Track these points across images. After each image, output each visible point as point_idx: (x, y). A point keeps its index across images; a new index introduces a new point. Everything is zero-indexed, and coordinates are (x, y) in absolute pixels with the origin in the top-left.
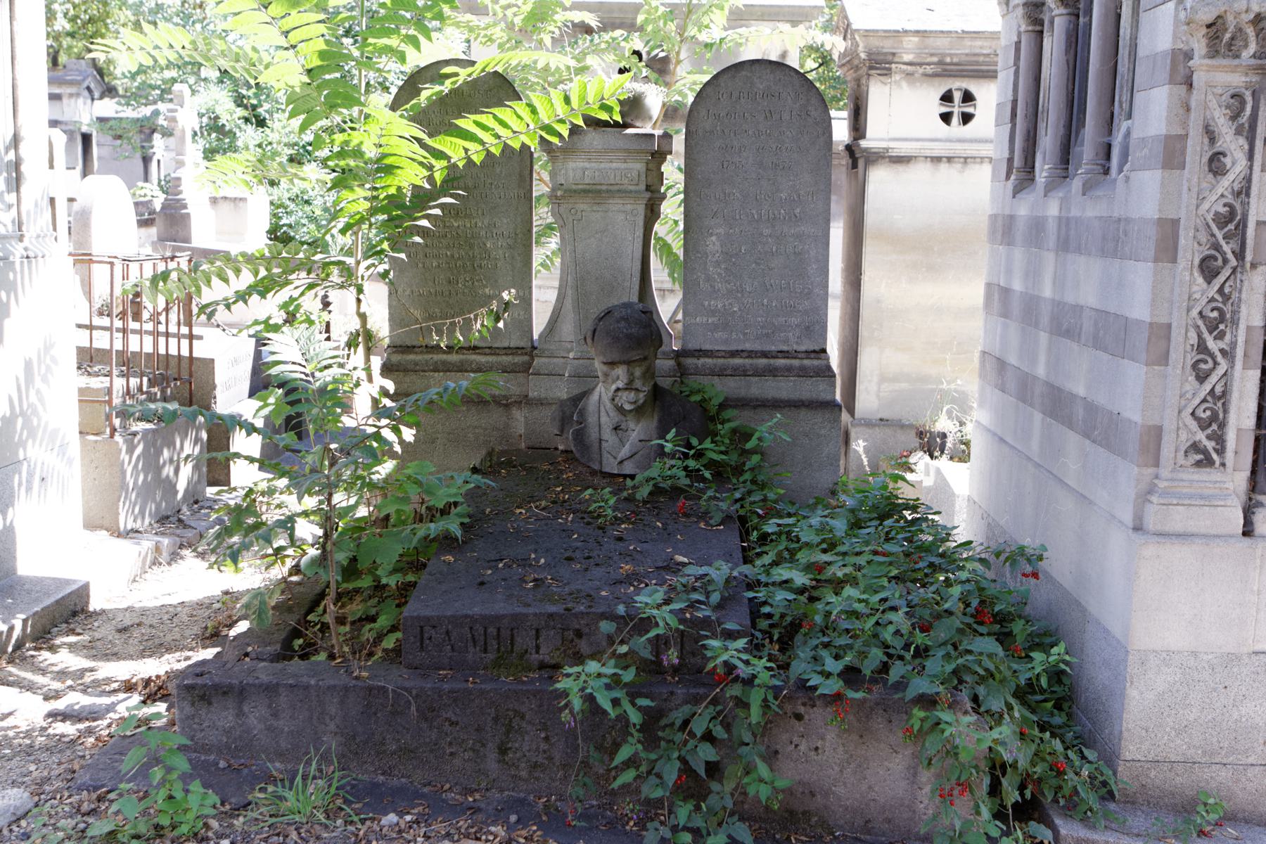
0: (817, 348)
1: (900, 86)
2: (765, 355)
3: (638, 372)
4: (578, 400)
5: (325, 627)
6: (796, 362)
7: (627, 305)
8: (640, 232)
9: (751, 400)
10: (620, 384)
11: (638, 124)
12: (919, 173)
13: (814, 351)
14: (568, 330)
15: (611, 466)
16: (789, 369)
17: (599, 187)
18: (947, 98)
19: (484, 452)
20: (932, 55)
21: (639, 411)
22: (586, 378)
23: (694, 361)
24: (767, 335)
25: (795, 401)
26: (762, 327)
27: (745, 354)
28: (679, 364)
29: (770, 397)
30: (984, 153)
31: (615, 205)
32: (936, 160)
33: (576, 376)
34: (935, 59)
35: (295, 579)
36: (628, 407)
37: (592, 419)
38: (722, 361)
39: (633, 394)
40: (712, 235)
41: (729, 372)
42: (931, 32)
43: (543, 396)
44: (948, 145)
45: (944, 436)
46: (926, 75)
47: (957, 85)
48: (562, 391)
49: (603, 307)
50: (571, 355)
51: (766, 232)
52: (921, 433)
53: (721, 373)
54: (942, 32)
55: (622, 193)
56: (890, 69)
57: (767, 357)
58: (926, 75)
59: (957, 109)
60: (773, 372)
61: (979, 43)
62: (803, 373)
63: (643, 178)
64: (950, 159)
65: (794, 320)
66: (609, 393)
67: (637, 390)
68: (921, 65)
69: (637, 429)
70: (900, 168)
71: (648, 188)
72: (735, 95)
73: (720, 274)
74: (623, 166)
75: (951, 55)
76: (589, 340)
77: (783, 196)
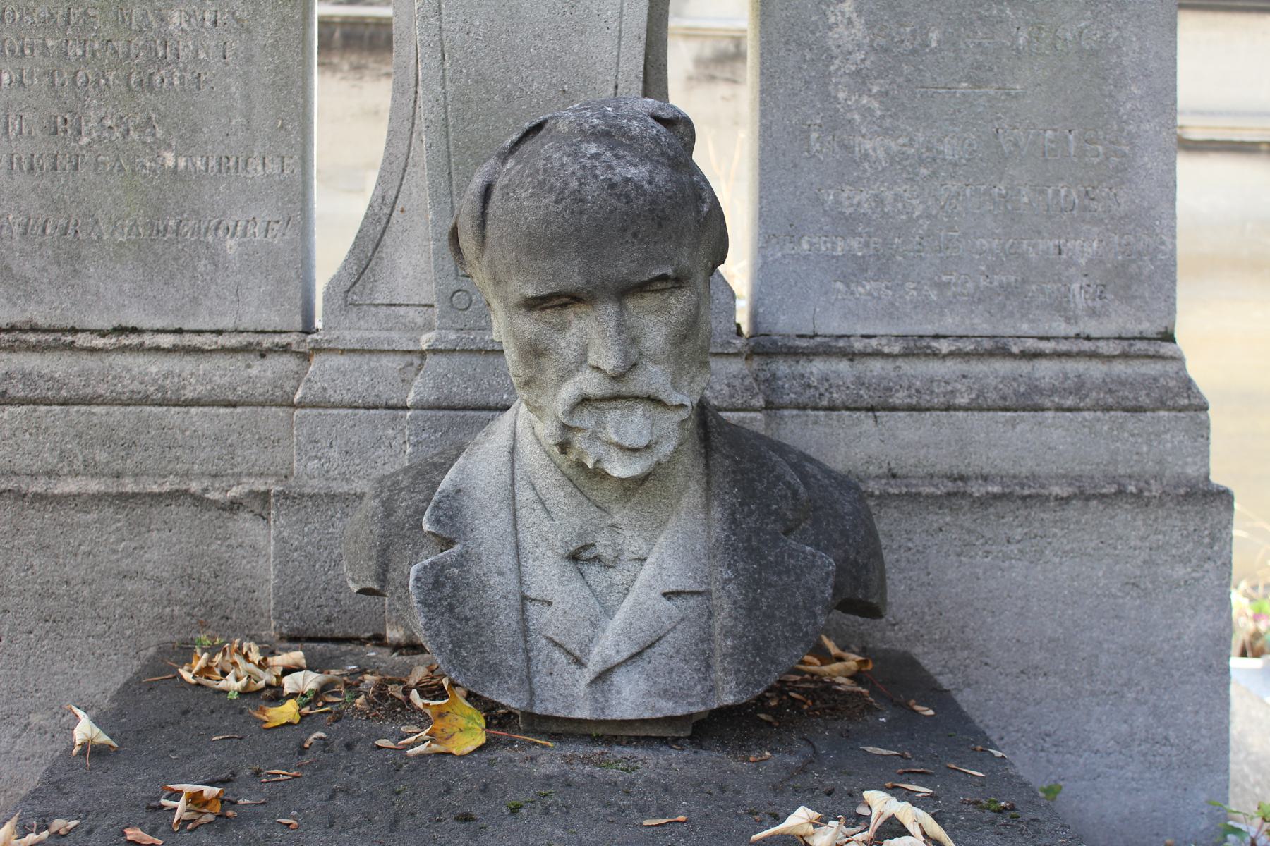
0: (1149, 328)
10: (588, 382)
19: (178, 638)
35: (1041, 794)
60: (1027, 402)
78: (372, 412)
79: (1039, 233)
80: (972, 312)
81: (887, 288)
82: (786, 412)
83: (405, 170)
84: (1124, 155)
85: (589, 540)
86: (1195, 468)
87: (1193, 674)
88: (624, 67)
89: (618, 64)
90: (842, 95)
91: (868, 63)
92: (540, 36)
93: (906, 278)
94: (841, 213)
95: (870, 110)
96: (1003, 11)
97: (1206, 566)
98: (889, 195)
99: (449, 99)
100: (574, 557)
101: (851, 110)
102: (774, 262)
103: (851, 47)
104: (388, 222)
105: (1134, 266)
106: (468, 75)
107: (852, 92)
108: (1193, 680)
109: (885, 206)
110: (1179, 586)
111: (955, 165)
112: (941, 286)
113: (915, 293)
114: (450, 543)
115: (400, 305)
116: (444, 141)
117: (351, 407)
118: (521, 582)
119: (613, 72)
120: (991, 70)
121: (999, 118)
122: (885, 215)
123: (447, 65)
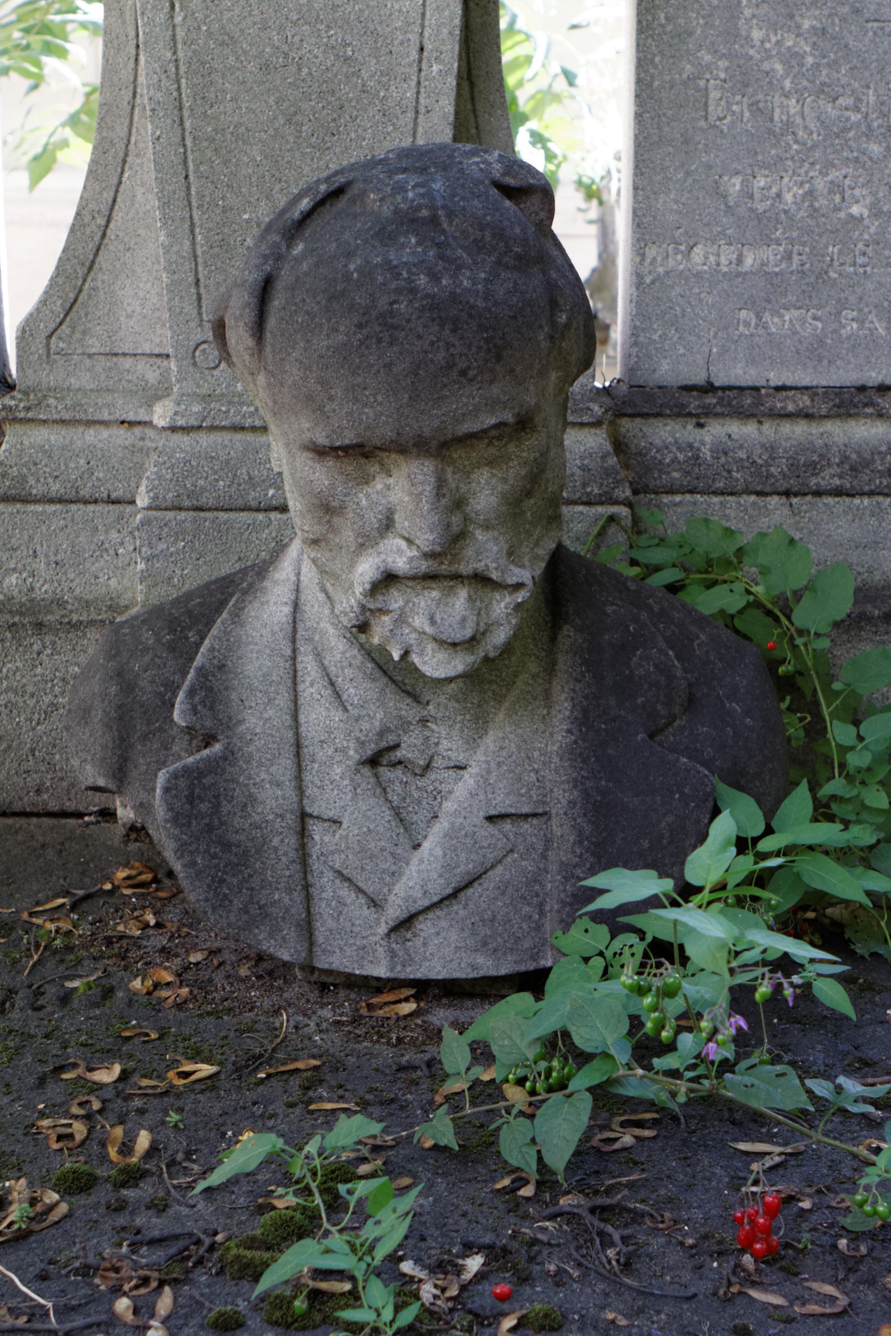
3: (485, 493)
4: (198, 614)
5: (662, 26)
7: (417, 160)
10: (399, 555)
14: (144, 304)
15: (355, 942)
21: (487, 681)
22: (224, 506)
23: (686, 432)
28: (619, 446)
33: (186, 502)
36: (434, 664)
37: (259, 720)
38: (798, 430)
41: (828, 478)
43: (43, 590)
48: (128, 573)
49: (313, 169)
50: (161, 414)
53: (798, 482)
66: (344, 591)
67: (481, 580)
69: (477, 762)
73: (792, 58)
76: (239, 337)
78: (91, 508)
81: (815, 318)
82: (666, 499)
83: (124, 161)
85: (391, 739)
89: (423, 15)
90: (757, 35)
93: (842, 305)
94: (751, 210)
98: (820, 184)
99: (183, 69)
100: (373, 762)
101: (769, 57)
102: (653, 282)
104: (104, 235)
106: (209, 33)
107: (774, 28)
113: (855, 325)
114: (208, 740)
115: (124, 355)
116: (178, 132)
117: (60, 501)
118: (300, 790)
119: (417, 29)
122: (814, 212)
123: (178, 19)
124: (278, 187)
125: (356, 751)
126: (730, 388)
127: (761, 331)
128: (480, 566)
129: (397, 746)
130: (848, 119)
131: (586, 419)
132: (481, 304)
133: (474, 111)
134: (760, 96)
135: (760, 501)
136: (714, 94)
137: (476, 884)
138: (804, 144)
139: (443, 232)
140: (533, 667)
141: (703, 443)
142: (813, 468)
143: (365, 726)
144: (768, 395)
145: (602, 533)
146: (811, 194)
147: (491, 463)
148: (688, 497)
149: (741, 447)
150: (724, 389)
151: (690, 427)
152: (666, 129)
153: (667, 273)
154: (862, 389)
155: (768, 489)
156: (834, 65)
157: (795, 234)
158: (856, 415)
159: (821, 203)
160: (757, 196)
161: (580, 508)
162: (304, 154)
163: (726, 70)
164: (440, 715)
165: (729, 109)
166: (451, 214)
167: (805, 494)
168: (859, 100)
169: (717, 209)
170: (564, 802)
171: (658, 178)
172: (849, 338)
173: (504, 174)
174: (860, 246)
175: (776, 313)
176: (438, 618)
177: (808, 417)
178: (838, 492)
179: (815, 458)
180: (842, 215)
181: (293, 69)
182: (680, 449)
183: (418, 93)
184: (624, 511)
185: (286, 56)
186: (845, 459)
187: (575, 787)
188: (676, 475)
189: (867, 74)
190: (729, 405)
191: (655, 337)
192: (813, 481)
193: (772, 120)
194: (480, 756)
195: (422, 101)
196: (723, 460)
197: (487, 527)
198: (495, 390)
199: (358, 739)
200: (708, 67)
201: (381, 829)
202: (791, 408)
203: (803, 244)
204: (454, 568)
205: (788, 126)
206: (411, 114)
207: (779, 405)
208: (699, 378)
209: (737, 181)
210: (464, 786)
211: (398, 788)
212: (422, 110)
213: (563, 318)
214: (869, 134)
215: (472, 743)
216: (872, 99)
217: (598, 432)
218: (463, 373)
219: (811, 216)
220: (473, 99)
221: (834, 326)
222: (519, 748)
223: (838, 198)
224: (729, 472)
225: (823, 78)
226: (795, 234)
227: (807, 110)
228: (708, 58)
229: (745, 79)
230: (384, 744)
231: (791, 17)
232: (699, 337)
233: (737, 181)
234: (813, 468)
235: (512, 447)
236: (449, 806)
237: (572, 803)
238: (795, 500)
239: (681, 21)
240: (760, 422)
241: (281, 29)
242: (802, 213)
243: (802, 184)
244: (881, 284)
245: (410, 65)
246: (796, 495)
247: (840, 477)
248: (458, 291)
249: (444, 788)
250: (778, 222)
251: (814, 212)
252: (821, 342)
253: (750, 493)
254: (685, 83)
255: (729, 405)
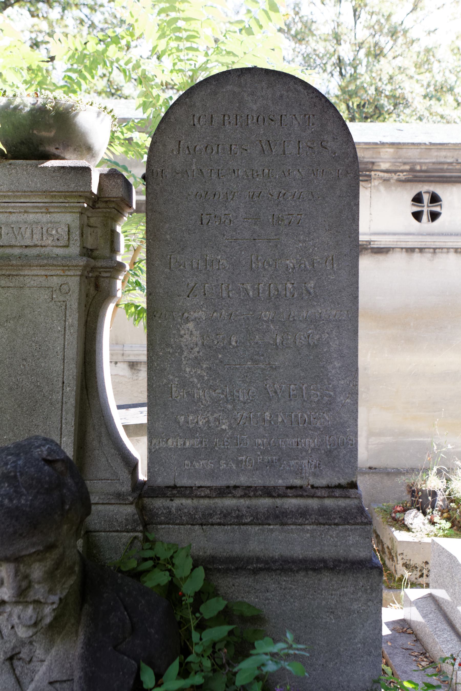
0: (343, 481)
1: (378, 190)
2: (268, 492)
3: (37, 571)
6: (313, 503)
8: (73, 319)
9: (249, 560)
11: (67, 157)
12: (397, 261)
13: (339, 486)
16: (303, 514)
17: (8, 251)
18: (418, 199)
20: (405, 164)
24: (271, 464)
25: (313, 561)
26: (263, 453)
27: (239, 492)
28: (142, 509)
29: (276, 555)
30: (449, 245)
31: (34, 277)
32: (410, 250)
34: (407, 167)
38: (206, 502)
39: (30, 610)
40: (187, 320)
41: (215, 519)
42: (404, 144)
44: (420, 238)
45: (434, 494)
46: (400, 181)
47: (426, 189)
51: (267, 315)
52: (414, 491)
54: (413, 144)
55: (46, 262)
56: (370, 176)
57: (270, 495)
58: (400, 181)
59: (426, 208)
60: (280, 517)
61: (443, 153)
62: (325, 518)
63: (76, 235)
64: (421, 250)
65: (309, 442)
67: (37, 602)
68: (395, 172)
70: (380, 257)
71: (88, 252)
72: (217, 119)
73: (200, 377)
74: (45, 218)
75: (420, 164)
77: (290, 263)
79: (287, 436)
80: (253, 474)
81: (211, 463)
82: (159, 527)
84: (331, 396)
85: (17, 650)
86: (364, 553)
87: (362, 657)
88: (66, 373)
89: (64, 372)
90: (188, 370)
91: (201, 353)
92: (25, 360)
93: (220, 459)
94: (188, 427)
95: (203, 377)
96: (269, 326)
97: (369, 604)
98: (211, 418)
100: (11, 659)
101: (192, 377)
102: (155, 451)
103: (192, 345)
105: (336, 451)
108: (362, 659)
109: (210, 423)
110: (354, 613)
111: (245, 403)
112: (239, 463)
119: (61, 376)
120: (263, 355)
121: (267, 379)
122: (209, 428)
124: (16, 428)
125: (3, 656)
126: (182, 487)
127: (192, 468)
128: (36, 598)
129: (19, 653)
130: (220, 397)
131: (127, 502)
132: (28, 509)
133: (88, 398)
134: (190, 390)
135: (192, 527)
136: (174, 389)
137: (294, 490)
138: (205, 405)
139: (18, 481)
140: (73, 621)
141: (172, 506)
142: (211, 515)
143: (8, 645)
144: (195, 490)
145: (132, 543)
146: (208, 422)
147: (40, 561)
148: (167, 526)
149: (186, 508)
150: (180, 487)
151: (168, 501)
152: (158, 401)
153: (159, 448)
154: (228, 487)
155: (195, 523)
156: (214, 379)
157: (203, 435)
158: (226, 497)
159: (212, 424)
160: (190, 422)
161: (125, 534)
162: (24, 417)
163: (178, 381)
164: (37, 640)
165: (179, 394)
166: (22, 475)
167: (208, 525)
168: (224, 391)
169: (176, 427)
170: (78, 677)
171: (156, 417)
172: (223, 470)
173: (47, 456)
174: (226, 439)
175: (197, 461)
176: (22, 616)
177: (209, 497)
178: (219, 524)
179: (211, 512)
180: (219, 429)
181: (20, 389)
182: (164, 509)
183: (63, 397)
184: (140, 535)
185: (17, 385)
186: (221, 512)
187: (82, 671)
188: (163, 518)
189: (225, 382)
190: (181, 493)
191: (156, 470)
192: (210, 521)
193: (194, 397)
194: (49, 658)
195: (64, 400)
196: (179, 513)
197: (39, 583)
198: (34, 539)
199: (4, 651)
200: (172, 380)
201: (10, 687)
202: (203, 494)
203: (206, 438)
204: (25, 600)
205: (199, 399)
206: (60, 404)
207: (198, 493)
208: (172, 483)
209: (183, 417)
210: (43, 668)
211: (20, 669)
212: (64, 403)
213: (67, 507)
214: (227, 402)
215: (47, 651)
216: (228, 390)
217: (132, 506)
218: (21, 535)
219: (208, 429)
220: (87, 394)
221: (217, 466)
222: (64, 654)
223: (217, 423)
224: (181, 517)
225: (211, 384)
226: (203, 435)
227: (206, 394)
228: (171, 377)
229: (184, 384)
230: (14, 653)
231: (199, 364)
232: (171, 470)
233: (183, 417)
234: (211, 515)
235: (47, 555)
236: (37, 678)
237: (80, 678)
238: (204, 527)
239: (162, 366)
240: (192, 499)
241: (15, 377)
242: (205, 428)
243: (205, 418)
244: (233, 452)
245: (59, 388)
246: (205, 525)
247: (220, 519)
248: (19, 505)
249: (37, 669)
250: (197, 431)
251: (209, 428)
252: (213, 471)
253: (188, 524)
254: (164, 386)
255: (181, 493)
